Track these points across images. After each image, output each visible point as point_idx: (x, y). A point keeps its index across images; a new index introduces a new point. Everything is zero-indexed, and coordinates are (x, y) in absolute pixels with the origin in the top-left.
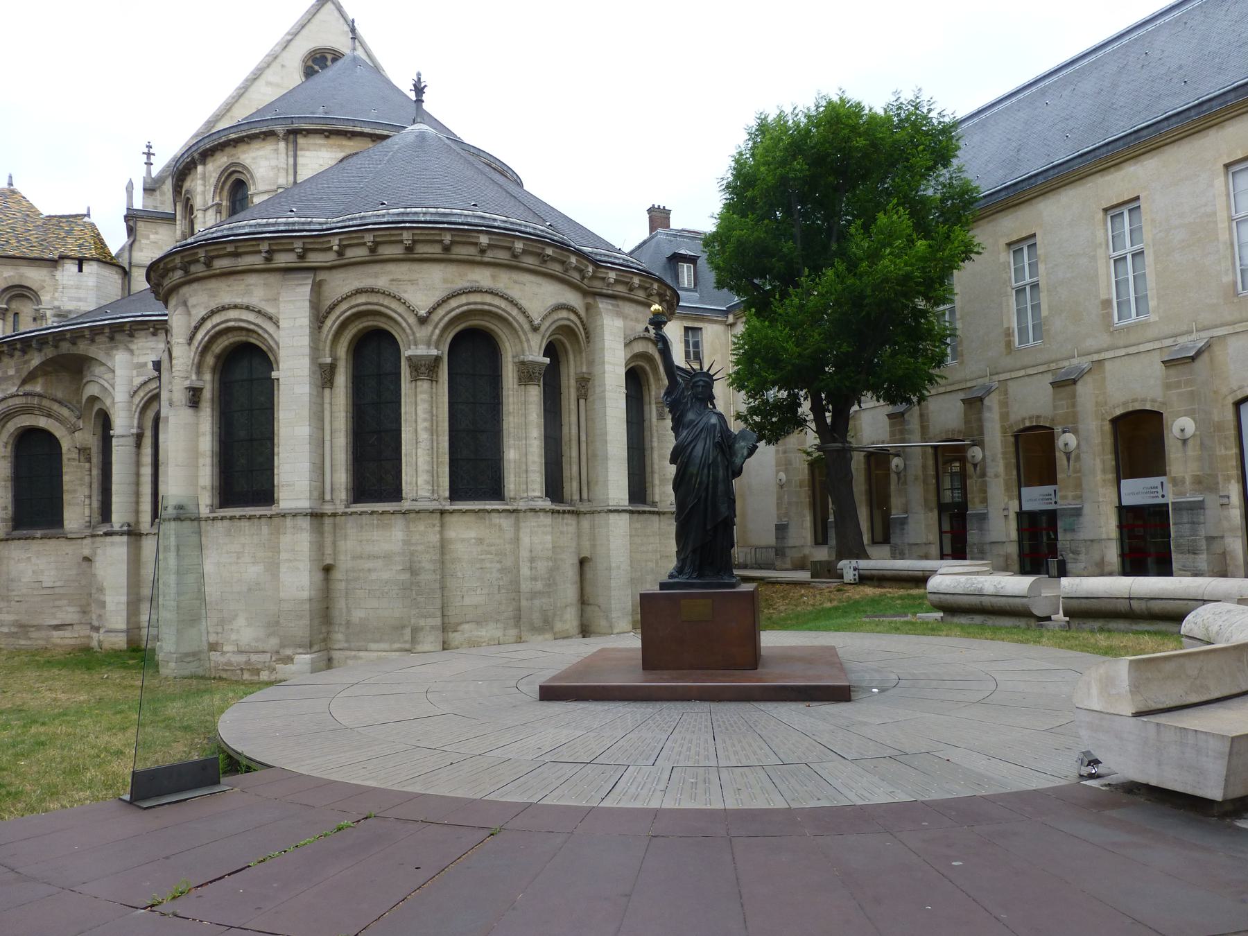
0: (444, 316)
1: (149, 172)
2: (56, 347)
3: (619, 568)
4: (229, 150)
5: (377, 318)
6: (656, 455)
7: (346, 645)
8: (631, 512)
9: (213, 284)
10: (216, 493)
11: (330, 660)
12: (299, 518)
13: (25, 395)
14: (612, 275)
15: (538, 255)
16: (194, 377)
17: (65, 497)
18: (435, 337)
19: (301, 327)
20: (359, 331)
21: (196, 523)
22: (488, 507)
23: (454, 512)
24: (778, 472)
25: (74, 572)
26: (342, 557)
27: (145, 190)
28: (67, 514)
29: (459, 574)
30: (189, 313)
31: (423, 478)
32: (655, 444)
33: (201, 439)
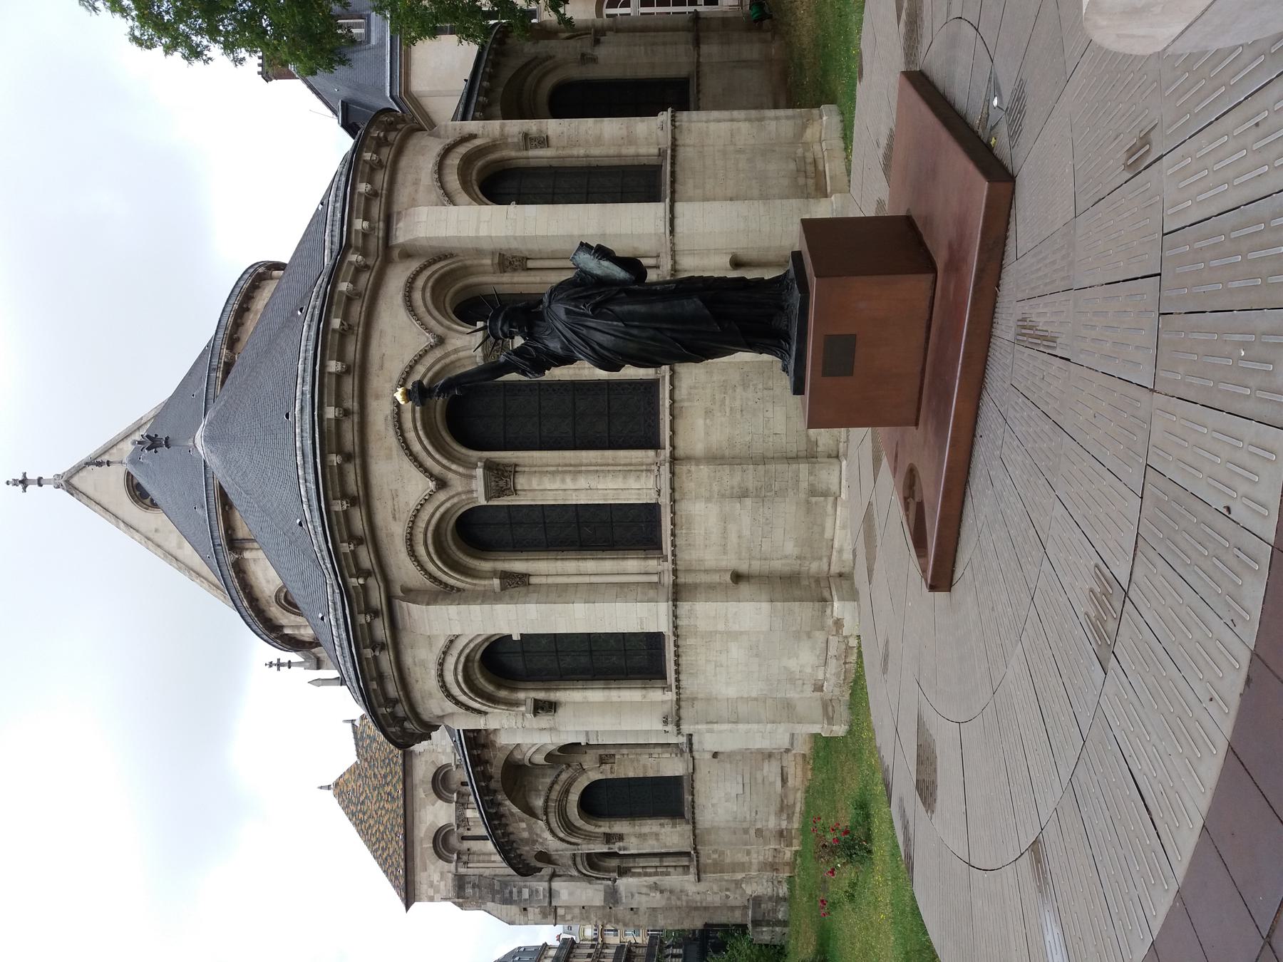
0: (434, 458)
1: (299, 664)
2: (495, 791)
4: (263, 604)
6: (595, 151)
7: (825, 560)
8: (673, 202)
9: (417, 695)
11: (840, 575)
12: (679, 612)
13: (546, 813)
16: (523, 709)
17: (652, 775)
18: (461, 470)
19: (459, 613)
20: (459, 548)
21: (683, 704)
22: (667, 402)
23: (673, 446)
25: (728, 766)
26: (724, 564)
27: (318, 668)
28: (668, 772)
29: (748, 438)
30: (452, 714)
31: (632, 483)
32: (582, 152)
33: (591, 699)
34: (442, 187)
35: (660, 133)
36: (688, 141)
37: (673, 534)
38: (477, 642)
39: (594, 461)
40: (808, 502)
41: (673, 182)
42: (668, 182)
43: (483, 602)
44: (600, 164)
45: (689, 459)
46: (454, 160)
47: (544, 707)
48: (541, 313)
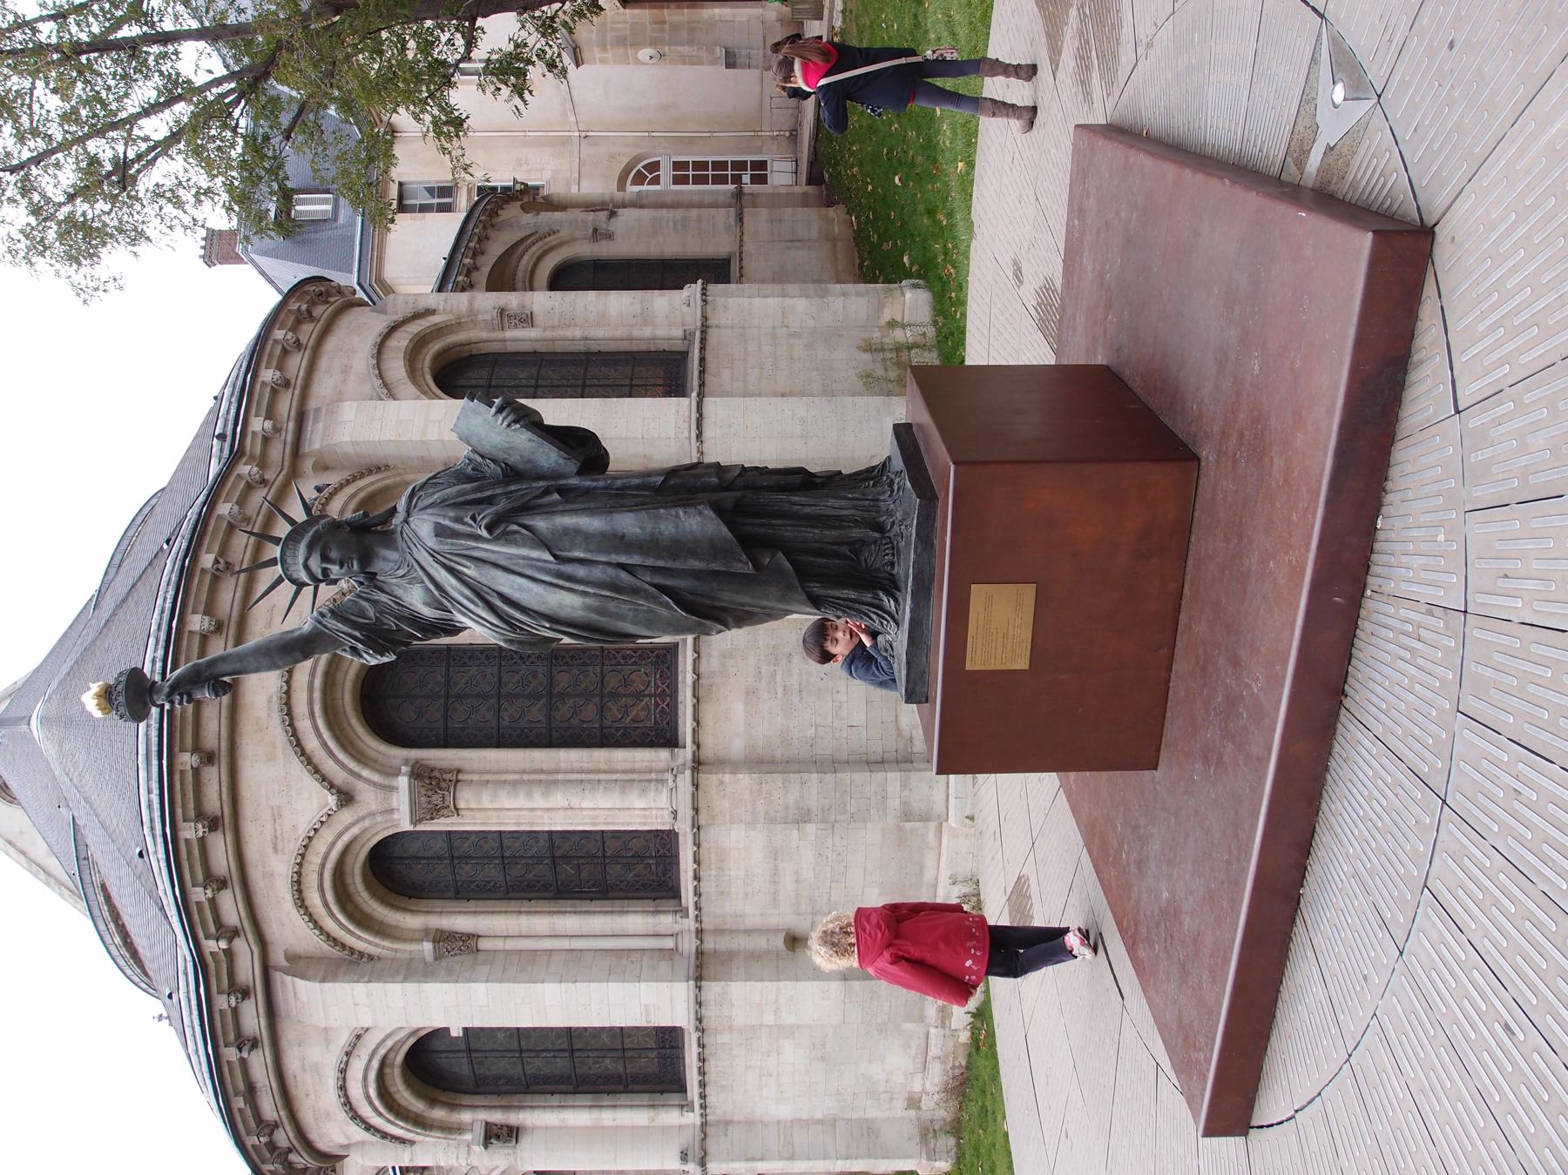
0: (337, 761)
3: (803, 421)
5: (348, 869)
6: (599, 333)
8: (701, 396)
9: (307, 1115)
10: (660, 1099)
14: (258, 424)
15: (216, 579)
16: (468, 1137)
18: (376, 777)
20: (374, 894)
21: (710, 1130)
24: (638, 62)
26: (774, 921)
29: (810, 732)
30: (363, 1143)
31: (636, 801)
32: (578, 333)
34: (381, 376)
35: (685, 308)
36: (723, 322)
37: (697, 878)
38: (396, 1038)
39: (577, 765)
40: (899, 829)
41: (702, 372)
42: (696, 373)
43: (405, 980)
44: (603, 349)
45: (722, 763)
46: (401, 341)
47: (497, 1135)
48: (392, 532)
